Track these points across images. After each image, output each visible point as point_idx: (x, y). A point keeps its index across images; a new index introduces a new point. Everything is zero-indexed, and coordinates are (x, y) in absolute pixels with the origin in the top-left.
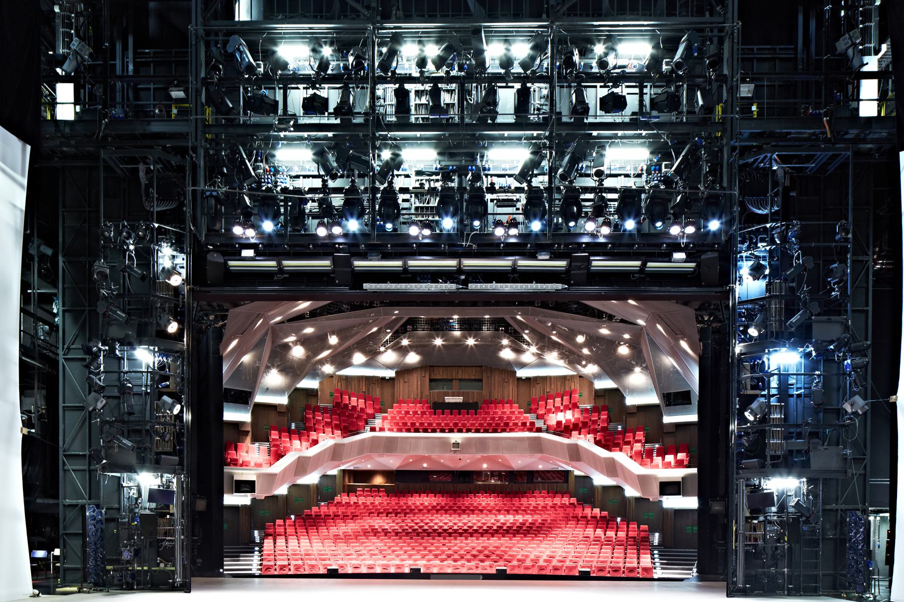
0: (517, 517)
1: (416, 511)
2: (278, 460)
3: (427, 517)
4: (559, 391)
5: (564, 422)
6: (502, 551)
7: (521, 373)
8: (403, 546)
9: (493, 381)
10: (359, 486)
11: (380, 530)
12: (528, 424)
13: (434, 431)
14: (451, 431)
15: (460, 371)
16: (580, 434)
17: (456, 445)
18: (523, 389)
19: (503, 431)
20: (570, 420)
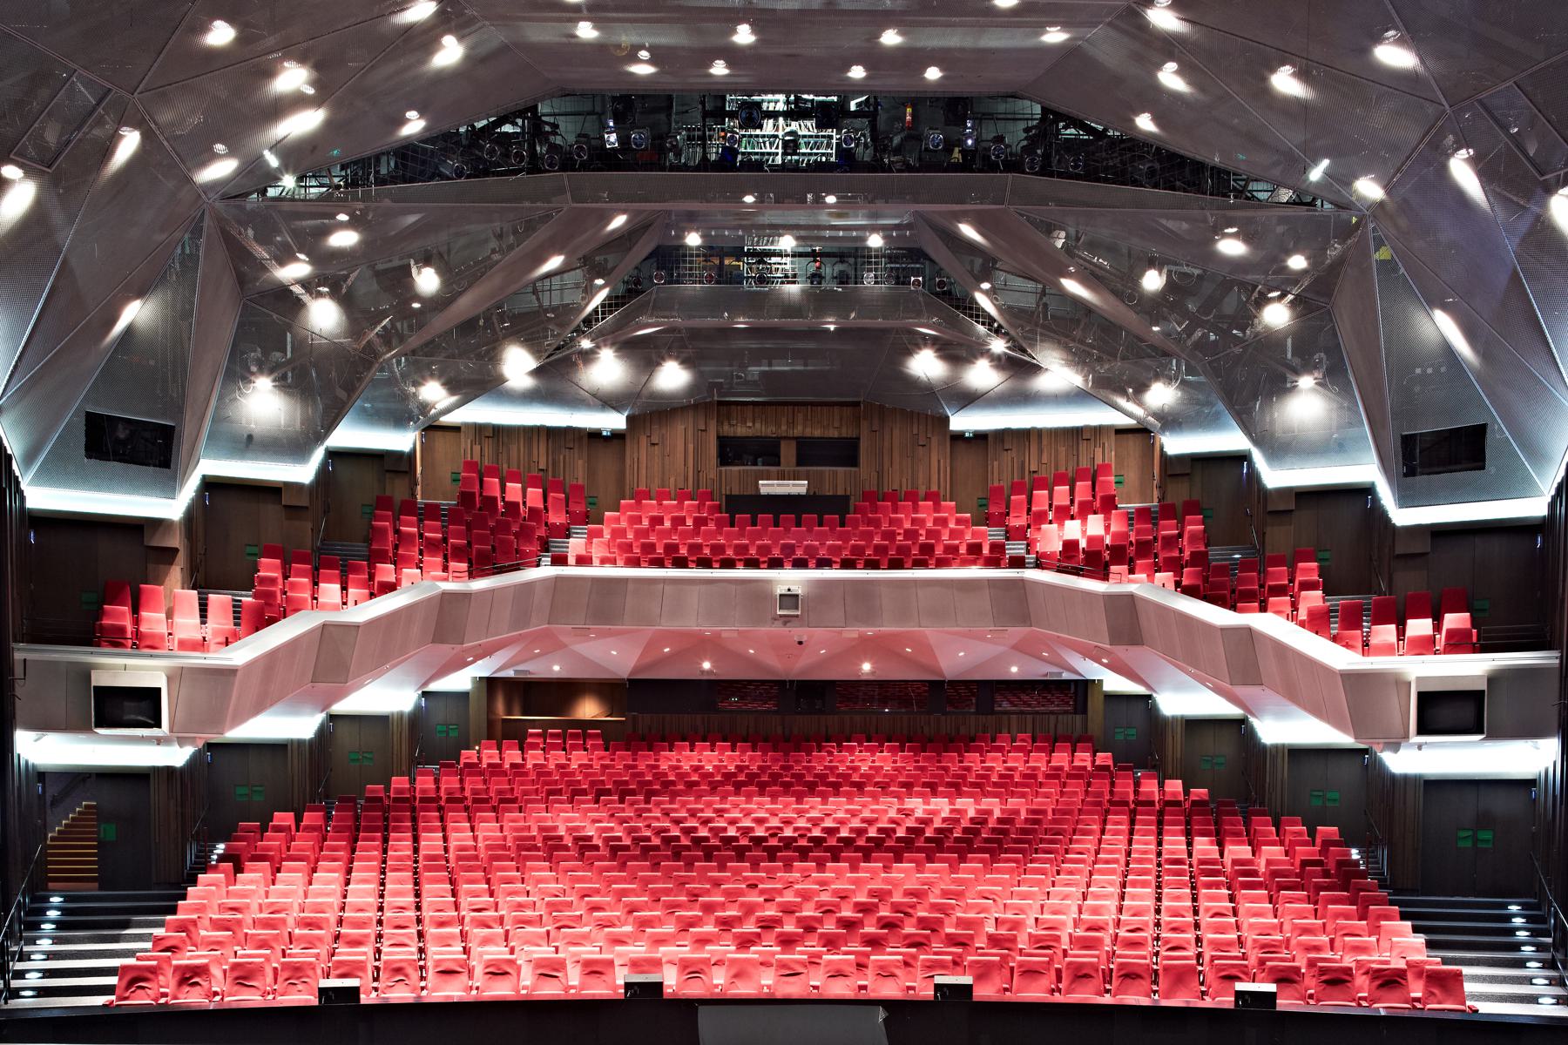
0: (961, 803)
1: (681, 787)
2: (257, 630)
3: (709, 804)
4: (1062, 470)
5: (1083, 544)
6: (935, 907)
7: (963, 421)
8: (625, 893)
9: (886, 444)
10: (533, 724)
11: (568, 842)
12: (986, 551)
13: (728, 564)
14: (776, 564)
15: (800, 417)
16: (1132, 571)
17: (790, 599)
18: (968, 460)
19: (920, 564)
20: (1101, 539)
